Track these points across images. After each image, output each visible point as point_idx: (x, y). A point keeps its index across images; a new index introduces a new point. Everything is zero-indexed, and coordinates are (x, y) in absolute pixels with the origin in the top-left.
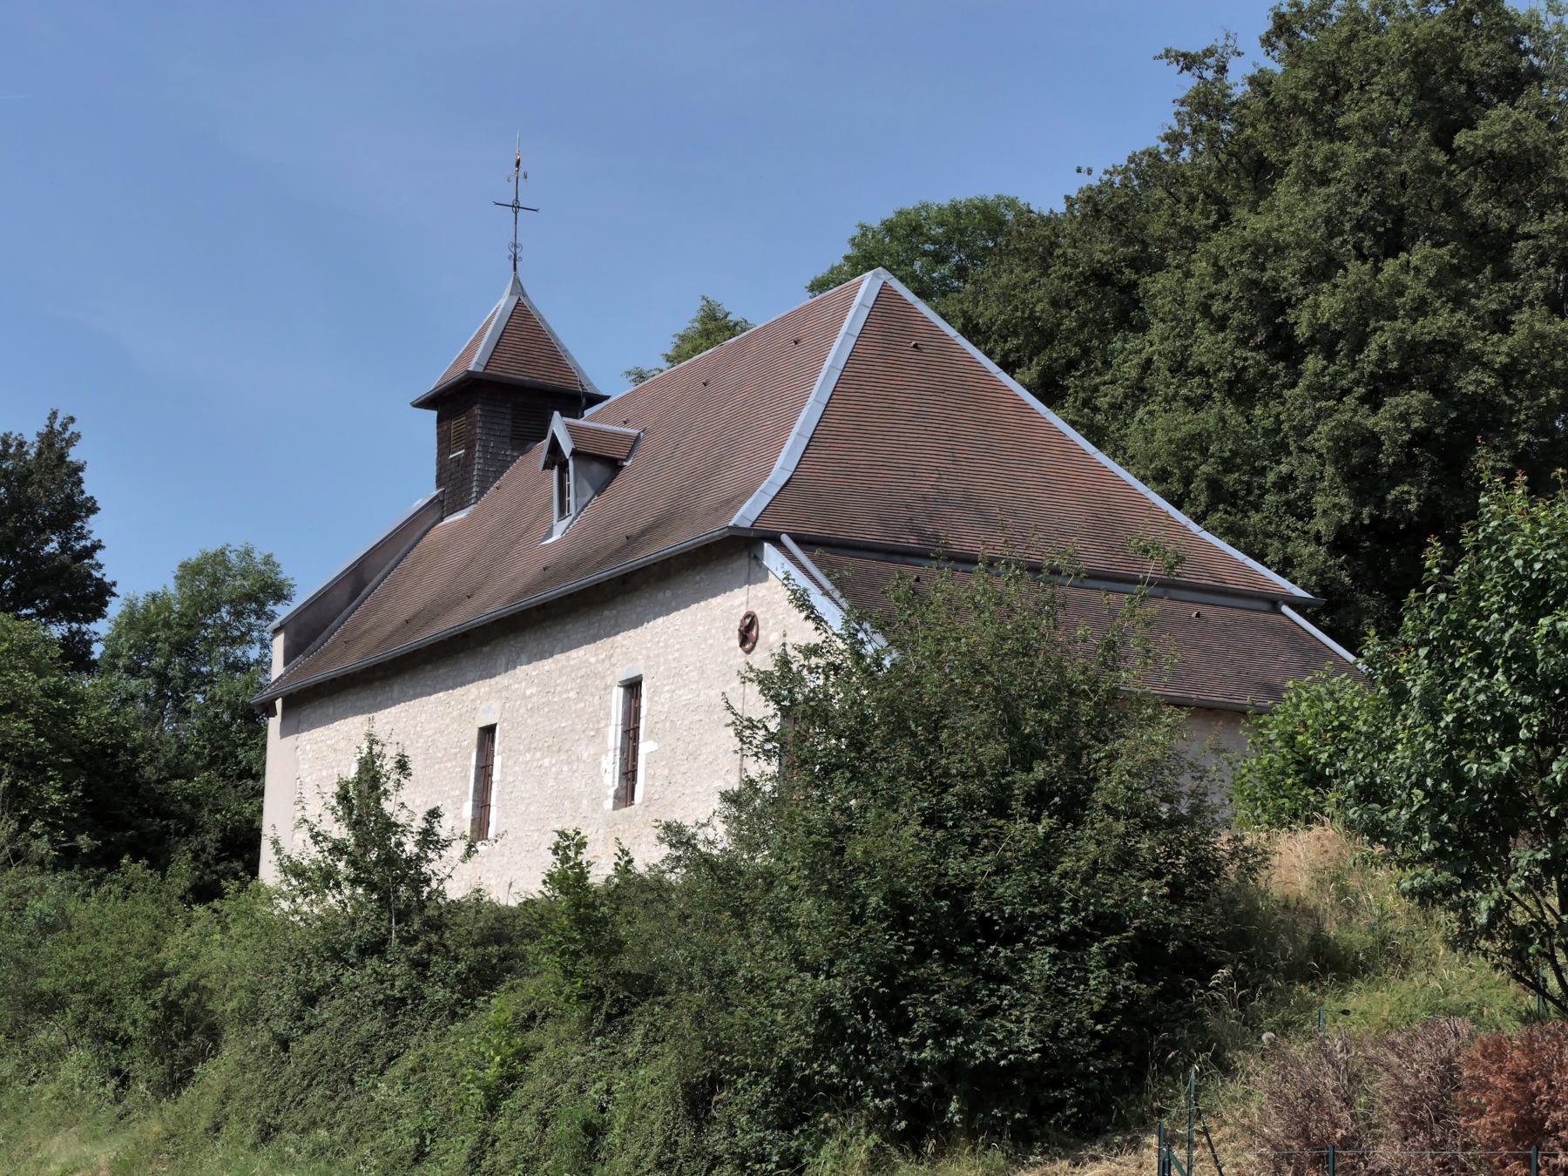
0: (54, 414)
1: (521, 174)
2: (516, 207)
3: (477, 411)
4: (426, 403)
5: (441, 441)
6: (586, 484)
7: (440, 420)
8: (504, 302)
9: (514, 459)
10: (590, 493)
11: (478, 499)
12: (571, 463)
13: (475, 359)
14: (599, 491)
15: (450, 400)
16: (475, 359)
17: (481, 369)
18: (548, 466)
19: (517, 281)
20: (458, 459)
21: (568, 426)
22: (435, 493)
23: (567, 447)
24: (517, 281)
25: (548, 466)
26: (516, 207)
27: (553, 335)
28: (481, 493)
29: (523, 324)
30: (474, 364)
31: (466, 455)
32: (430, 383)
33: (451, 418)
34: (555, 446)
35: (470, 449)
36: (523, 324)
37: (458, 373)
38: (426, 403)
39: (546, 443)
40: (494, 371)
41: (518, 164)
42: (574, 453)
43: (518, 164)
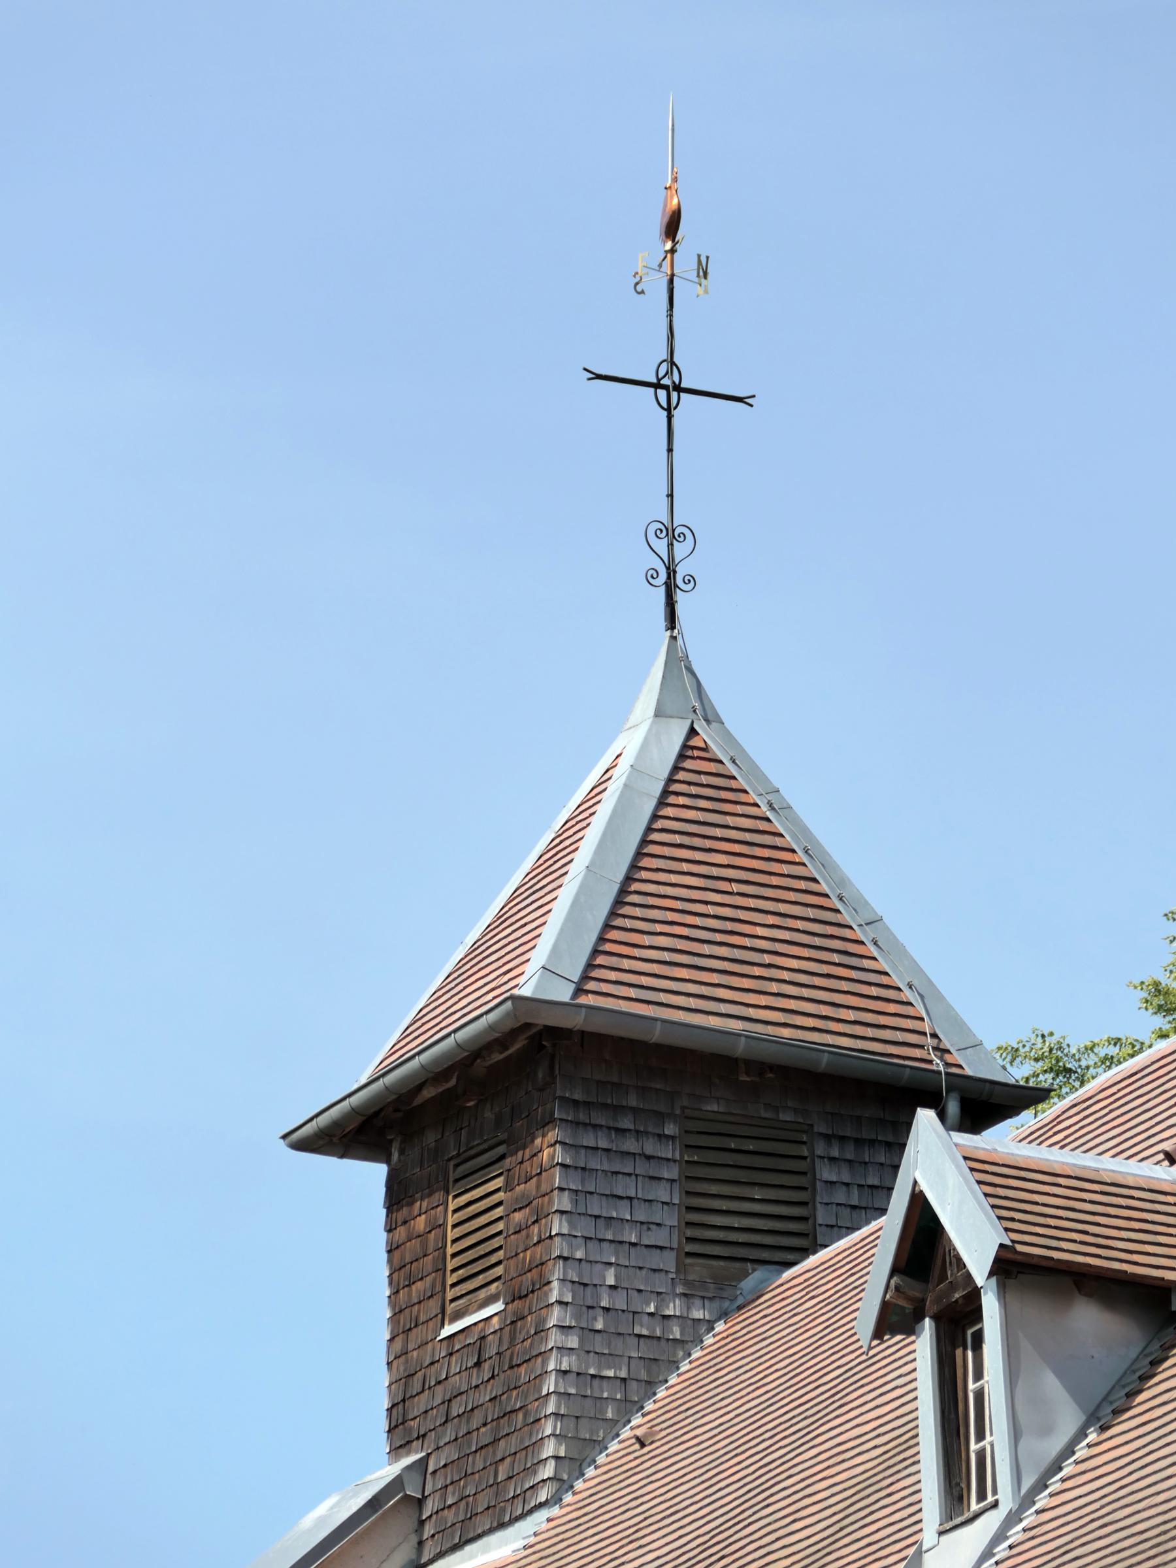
0: (699, 256)
1: (685, 263)
2: (669, 388)
3: (549, 1148)
4: (350, 1133)
5: (403, 1270)
6: (1051, 1384)
7: (398, 1196)
8: (637, 744)
9: (695, 1332)
10: (1069, 1419)
11: (563, 1484)
12: (990, 1305)
13: (539, 956)
14: (1104, 1411)
15: (427, 1127)
16: (539, 956)
17: (564, 993)
18: (894, 1321)
19: (679, 665)
20: (477, 1340)
21: (976, 1164)
22: (390, 1471)
23: (974, 1240)
24: (679, 665)
25: (894, 1321)
26: (669, 388)
27: (826, 864)
28: (574, 1464)
29: (706, 818)
30: (543, 971)
31: (513, 1322)
32: (354, 1061)
33: (441, 1184)
34: (924, 1238)
35: (524, 1294)
36: (706, 818)
37: (476, 1014)
38: (350, 1133)
39: (888, 1229)
40: (622, 1002)
41: (672, 227)
42: (1006, 1266)
43: (672, 227)
